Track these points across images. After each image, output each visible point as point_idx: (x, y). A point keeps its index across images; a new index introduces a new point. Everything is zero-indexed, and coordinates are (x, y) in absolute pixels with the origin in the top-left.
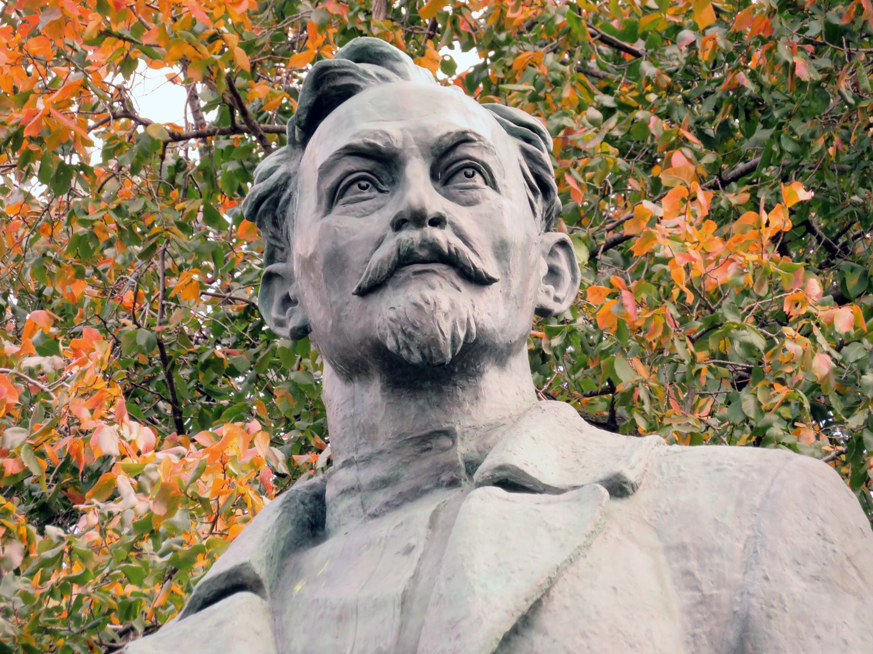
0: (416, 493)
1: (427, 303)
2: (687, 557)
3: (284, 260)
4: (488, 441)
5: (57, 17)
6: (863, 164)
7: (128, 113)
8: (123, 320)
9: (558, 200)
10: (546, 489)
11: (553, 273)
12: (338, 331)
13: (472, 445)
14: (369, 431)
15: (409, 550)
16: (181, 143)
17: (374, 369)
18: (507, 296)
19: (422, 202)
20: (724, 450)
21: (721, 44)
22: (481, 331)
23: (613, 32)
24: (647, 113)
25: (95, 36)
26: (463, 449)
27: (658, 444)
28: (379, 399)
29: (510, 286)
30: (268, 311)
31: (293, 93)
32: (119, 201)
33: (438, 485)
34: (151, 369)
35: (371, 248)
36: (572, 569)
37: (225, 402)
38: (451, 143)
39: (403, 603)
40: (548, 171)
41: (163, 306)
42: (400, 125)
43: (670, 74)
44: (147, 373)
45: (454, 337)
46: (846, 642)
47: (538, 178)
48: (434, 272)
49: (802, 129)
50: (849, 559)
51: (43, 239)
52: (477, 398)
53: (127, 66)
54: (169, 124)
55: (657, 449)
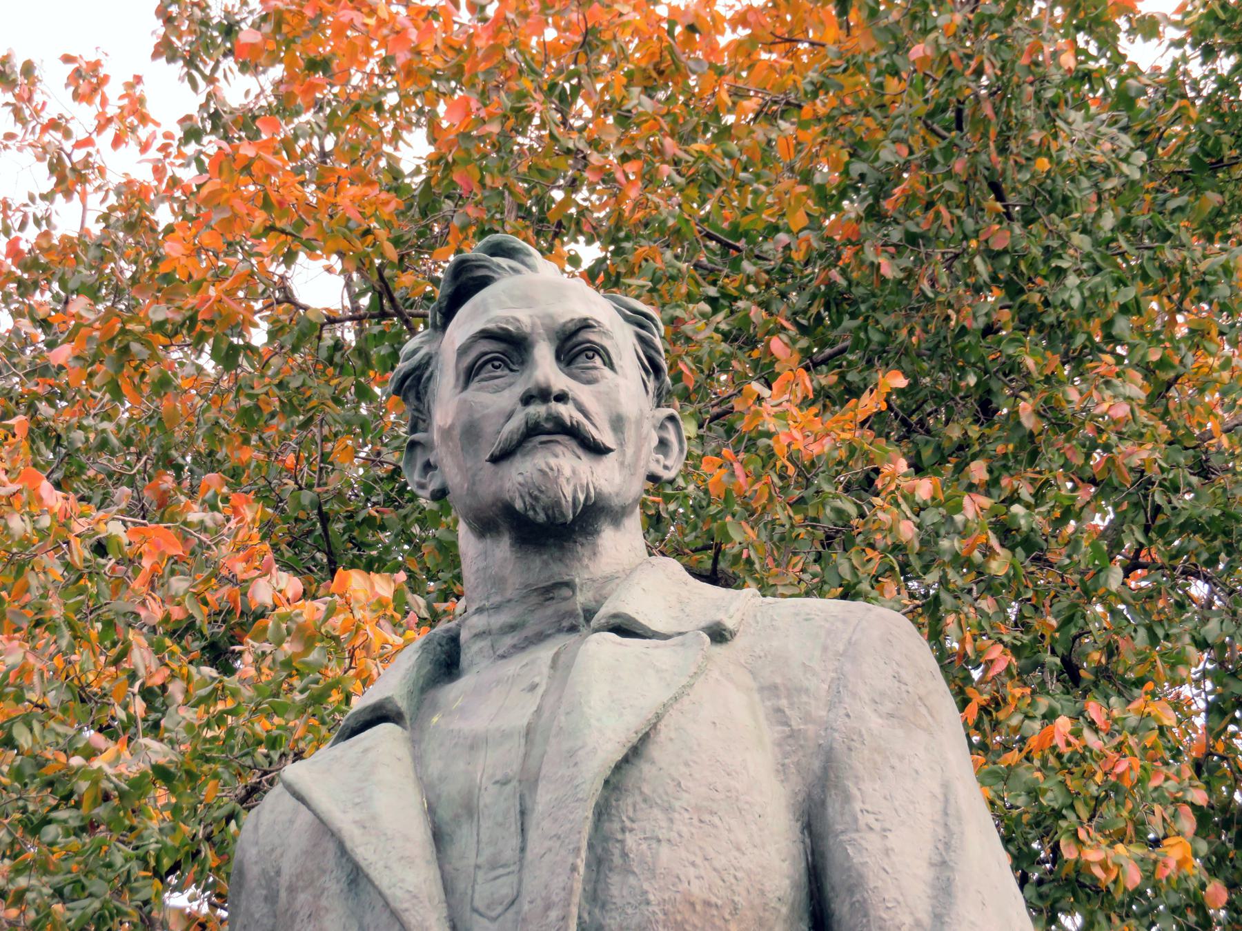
0: (540, 638)
1: (552, 469)
2: (778, 697)
3: (426, 430)
4: (604, 592)
5: (226, 215)
6: (940, 351)
7: (289, 298)
8: (285, 481)
9: (668, 379)
10: (654, 635)
11: (663, 444)
12: (472, 493)
13: (590, 595)
14: (498, 582)
15: (533, 687)
16: (337, 325)
17: (504, 527)
18: (622, 464)
19: (547, 380)
20: (815, 602)
21: (815, 244)
22: (599, 495)
23: (722, 231)
24: (749, 303)
25: (261, 230)
26: (582, 599)
27: (754, 596)
28: (508, 554)
29: (624, 455)
30: (411, 475)
31: (435, 282)
32: (280, 377)
33: (560, 631)
34: (309, 523)
35: (502, 421)
36: (677, 706)
37: (374, 553)
38: (574, 328)
39: (527, 734)
40: (659, 354)
41: (321, 469)
42: (529, 312)
43: (768, 272)
44: (306, 527)
45: (575, 499)
46: (917, 772)
47: (651, 360)
48: (557, 442)
49: (886, 321)
50: (920, 698)
51: (214, 410)
52: (595, 554)
53: (289, 258)
54: (326, 309)
55: (753, 600)
